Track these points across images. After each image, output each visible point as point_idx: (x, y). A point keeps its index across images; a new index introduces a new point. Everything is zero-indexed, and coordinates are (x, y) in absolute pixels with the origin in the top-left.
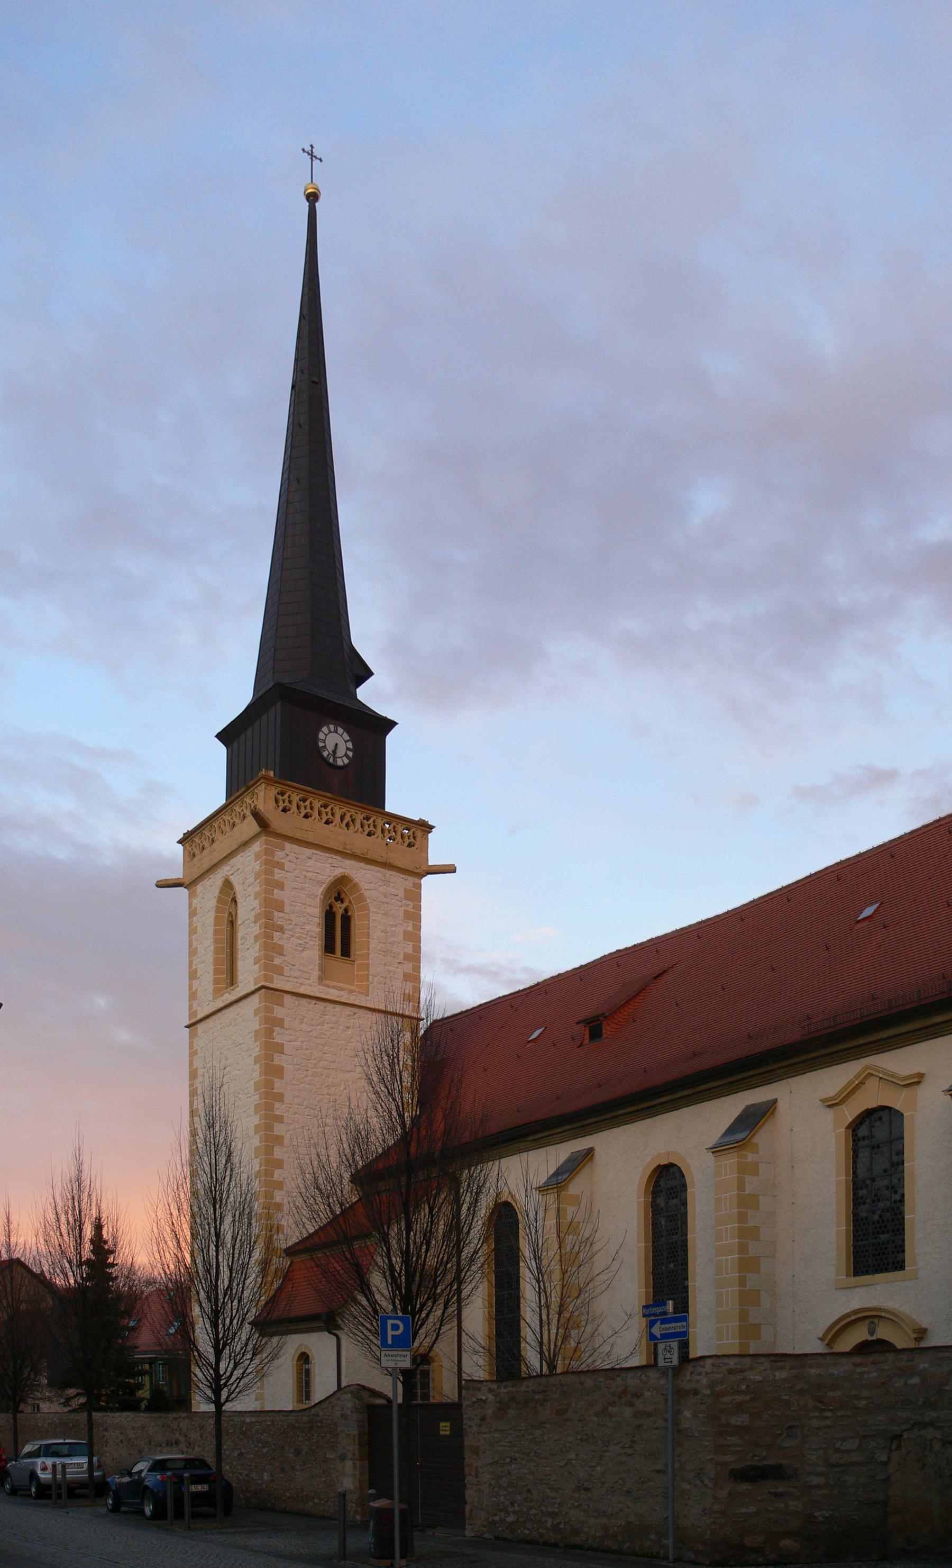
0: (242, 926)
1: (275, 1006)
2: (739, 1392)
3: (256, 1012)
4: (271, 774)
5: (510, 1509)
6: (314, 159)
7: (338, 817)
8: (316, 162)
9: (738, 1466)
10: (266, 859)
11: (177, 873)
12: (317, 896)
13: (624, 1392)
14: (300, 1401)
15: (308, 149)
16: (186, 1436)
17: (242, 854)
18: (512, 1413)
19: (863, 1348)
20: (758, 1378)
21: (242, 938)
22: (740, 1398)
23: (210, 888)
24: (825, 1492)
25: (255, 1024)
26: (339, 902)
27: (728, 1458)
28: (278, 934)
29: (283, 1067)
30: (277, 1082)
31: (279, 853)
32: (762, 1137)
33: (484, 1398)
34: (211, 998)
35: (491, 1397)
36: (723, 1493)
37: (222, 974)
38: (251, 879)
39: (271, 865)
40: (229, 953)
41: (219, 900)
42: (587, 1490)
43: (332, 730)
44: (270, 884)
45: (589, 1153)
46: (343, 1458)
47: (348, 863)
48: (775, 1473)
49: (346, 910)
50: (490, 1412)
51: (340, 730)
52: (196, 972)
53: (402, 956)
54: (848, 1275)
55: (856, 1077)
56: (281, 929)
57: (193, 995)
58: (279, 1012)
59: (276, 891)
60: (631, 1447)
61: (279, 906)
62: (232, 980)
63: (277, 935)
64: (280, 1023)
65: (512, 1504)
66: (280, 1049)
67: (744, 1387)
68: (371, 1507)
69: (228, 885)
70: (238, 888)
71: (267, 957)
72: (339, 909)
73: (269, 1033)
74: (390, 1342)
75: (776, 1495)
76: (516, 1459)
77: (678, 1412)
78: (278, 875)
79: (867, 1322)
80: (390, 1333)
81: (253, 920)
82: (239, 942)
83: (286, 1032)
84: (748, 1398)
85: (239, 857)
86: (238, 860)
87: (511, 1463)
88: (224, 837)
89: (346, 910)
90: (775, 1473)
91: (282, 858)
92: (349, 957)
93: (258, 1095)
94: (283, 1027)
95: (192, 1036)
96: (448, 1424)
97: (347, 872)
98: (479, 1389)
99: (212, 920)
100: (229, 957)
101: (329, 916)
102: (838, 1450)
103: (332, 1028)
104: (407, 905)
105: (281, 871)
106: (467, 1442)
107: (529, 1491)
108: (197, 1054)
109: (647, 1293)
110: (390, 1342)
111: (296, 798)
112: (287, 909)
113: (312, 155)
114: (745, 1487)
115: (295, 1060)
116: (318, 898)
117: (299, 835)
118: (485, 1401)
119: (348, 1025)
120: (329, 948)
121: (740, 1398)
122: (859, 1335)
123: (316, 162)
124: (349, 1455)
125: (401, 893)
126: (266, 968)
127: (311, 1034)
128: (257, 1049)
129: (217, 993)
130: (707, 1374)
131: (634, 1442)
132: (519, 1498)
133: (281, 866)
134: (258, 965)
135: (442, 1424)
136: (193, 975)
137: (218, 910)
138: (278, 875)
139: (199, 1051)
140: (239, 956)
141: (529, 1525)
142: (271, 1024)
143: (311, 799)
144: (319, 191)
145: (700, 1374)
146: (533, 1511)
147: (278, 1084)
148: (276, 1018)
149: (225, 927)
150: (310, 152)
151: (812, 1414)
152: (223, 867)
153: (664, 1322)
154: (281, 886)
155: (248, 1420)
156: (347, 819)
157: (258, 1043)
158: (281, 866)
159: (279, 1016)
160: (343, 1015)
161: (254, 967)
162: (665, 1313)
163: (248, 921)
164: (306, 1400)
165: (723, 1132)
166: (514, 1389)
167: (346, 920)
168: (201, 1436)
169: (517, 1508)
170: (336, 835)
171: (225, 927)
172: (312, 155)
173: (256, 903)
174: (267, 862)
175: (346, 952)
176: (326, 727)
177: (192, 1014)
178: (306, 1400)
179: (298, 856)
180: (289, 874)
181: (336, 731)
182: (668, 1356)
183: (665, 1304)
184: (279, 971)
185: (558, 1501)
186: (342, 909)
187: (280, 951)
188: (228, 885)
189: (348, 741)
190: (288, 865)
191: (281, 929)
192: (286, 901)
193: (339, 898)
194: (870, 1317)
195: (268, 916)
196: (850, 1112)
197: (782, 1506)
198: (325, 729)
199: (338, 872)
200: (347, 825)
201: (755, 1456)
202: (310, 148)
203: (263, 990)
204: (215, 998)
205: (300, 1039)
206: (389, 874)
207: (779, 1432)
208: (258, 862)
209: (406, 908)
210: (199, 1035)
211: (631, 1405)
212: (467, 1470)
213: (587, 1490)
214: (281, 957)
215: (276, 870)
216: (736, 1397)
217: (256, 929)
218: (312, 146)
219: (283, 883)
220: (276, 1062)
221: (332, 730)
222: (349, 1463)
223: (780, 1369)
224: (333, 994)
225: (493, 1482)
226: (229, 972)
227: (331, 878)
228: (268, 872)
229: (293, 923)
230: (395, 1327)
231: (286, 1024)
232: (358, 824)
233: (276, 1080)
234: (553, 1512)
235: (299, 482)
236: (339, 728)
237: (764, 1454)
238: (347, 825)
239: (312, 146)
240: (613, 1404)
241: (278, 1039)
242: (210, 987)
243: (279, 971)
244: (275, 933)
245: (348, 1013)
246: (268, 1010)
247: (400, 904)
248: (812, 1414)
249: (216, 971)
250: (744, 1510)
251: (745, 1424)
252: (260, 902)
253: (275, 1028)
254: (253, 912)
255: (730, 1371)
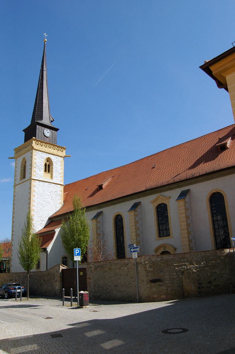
5: (98, 292)
9: (151, 279)
11: (13, 156)
14: (37, 269)
16: (15, 278)
18: (98, 269)
19: (163, 253)
20: (154, 260)
23: (20, 160)
24: (170, 285)
32: (138, 209)
33: (91, 266)
35: (93, 266)
36: (148, 286)
42: (117, 286)
45: (102, 212)
46: (56, 281)
48: (159, 280)
50: (93, 270)
54: (158, 237)
55: (157, 197)
57: (15, 180)
62: (24, 177)
65: (99, 291)
68: (87, 291)
74: (76, 255)
76: (99, 280)
79: (164, 247)
90: (159, 280)
95: (15, 188)
96: (82, 273)
97: (49, 157)
98: (90, 264)
102: (172, 275)
106: (87, 276)
109: (115, 242)
110: (76, 255)
118: (91, 267)
120: (45, 171)
122: (162, 250)
124: (58, 281)
129: (21, 180)
132: (100, 289)
135: (81, 273)
136: (15, 176)
141: (103, 295)
146: (104, 292)
151: (166, 268)
153: (133, 248)
155: (32, 274)
156: (50, 146)
165: (131, 207)
166: (98, 264)
168: (19, 278)
169: (100, 291)
170: (48, 150)
177: (15, 184)
185: (110, 289)
194: (164, 246)
196: (156, 204)
199: (47, 157)
211: (126, 266)
212: (87, 283)
213: (117, 286)
222: (58, 283)
225: (94, 286)
230: (77, 251)
234: (109, 292)
240: (122, 267)
248: (166, 268)
249: (21, 175)
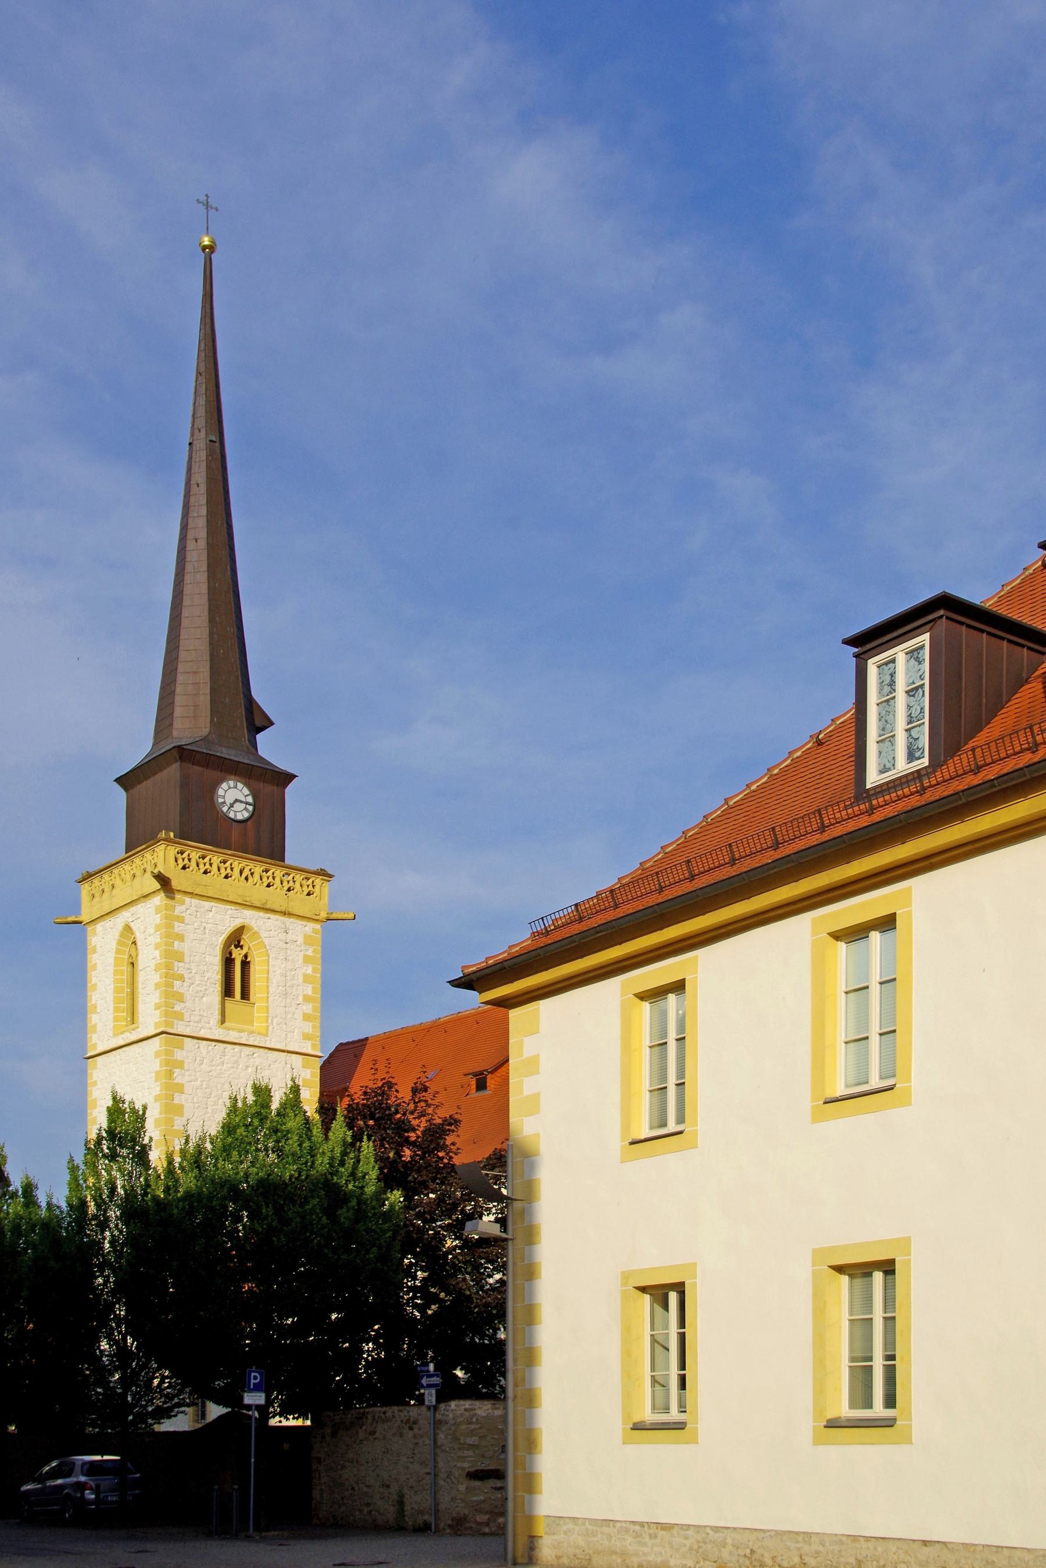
0: (143, 972)
1: (175, 1050)
2: (471, 1423)
3: (157, 1054)
4: (172, 834)
6: (209, 209)
7: (236, 872)
8: (212, 212)
10: (166, 914)
12: (216, 946)
13: (408, 1421)
15: (203, 199)
17: (143, 904)
20: (484, 1414)
21: (142, 984)
22: (473, 1427)
25: (156, 1065)
26: (239, 949)
27: (466, 1465)
28: (179, 982)
29: (183, 1105)
30: (178, 1119)
31: (179, 908)
34: (111, 1034)
37: (123, 1012)
38: (152, 931)
39: (171, 919)
40: (129, 993)
41: (120, 943)
43: (232, 786)
44: (171, 936)
47: (248, 913)
49: (246, 956)
51: (240, 785)
52: (96, 1007)
53: (301, 998)
56: (182, 978)
58: (179, 1055)
59: (176, 943)
60: (413, 1457)
61: (180, 957)
63: (177, 983)
64: (180, 1065)
66: (180, 1088)
67: (474, 1420)
69: (128, 928)
70: (139, 937)
71: (167, 1005)
72: (238, 955)
73: (170, 1074)
74: (252, 1387)
75: (496, 1489)
77: (435, 1435)
78: (178, 928)
80: (253, 1381)
81: (154, 968)
82: (140, 986)
83: (187, 1073)
84: (477, 1427)
85: (139, 906)
86: (140, 908)
87: (342, 1469)
88: (124, 886)
89: (246, 956)
91: (182, 912)
92: (249, 1000)
93: (158, 1132)
94: (182, 1068)
97: (247, 922)
99: (112, 961)
100: (129, 997)
101: (228, 962)
103: (232, 1068)
104: (307, 950)
105: (180, 924)
107: (353, 1488)
108: (96, 1085)
110: (252, 1387)
111: (195, 855)
112: (187, 960)
113: (207, 206)
114: (477, 1483)
115: (195, 1099)
116: (218, 948)
117: (197, 891)
119: (247, 1064)
120: (228, 991)
121: (473, 1427)
123: (212, 212)
125: (300, 940)
126: (166, 1014)
127: (211, 1074)
128: (158, 1089)
130: (452, 1411)
131: (414, 1454)
133: (181, 920)
134: (159, 1011)
137: (118, 951)
138: (178, 928)
139: (99, 1083)
140: (140, 1000)
142: (171, 1066)
143: (210, 856)
144: (215, 244)
145: (448, 1411)
147: (178, 1076)
148: (176, 1061)
149: (125, 968)
150: (205, 202)
152: (123, 913)
154: (181, 938)
156: (246, 872)
157: (158, 1083)
158: (181, 920)
159: (179, 1058)
160: (242, 1055)
161: (154, 1012)
162: (428, 1371)
163: (149, 968)
164: (202, 1419)
167: (245, 964)
170: (236, 887)
171: (125, 968)
172: (207, 206)
173: (157, 953)
174: (167, 917)
175: (245, 995)
176: (225, 783)
178: (202, 1419)
179: (198, 909)
180: (189, 927)
181: (236, 787)
182: (430, 1398)
183: (428, 1366)
184: (180, 1016)
186: (242, 956)
187: (181, 998)
188: (128, 928)
189: (247, 795)
190: (187, 919)
191: (182, 978)
192: (186, 952)
193: (238, 945)
195: (169, 967)
197: (500, 1496)
198: (224, 786)
199: (237, 923)
200: (247, 879)
201: (482, 1463)
202: (205, 198)
203: (164, 1035)
204: (115, 1035)
205: (199, 1080)
206: (289, 921)
207: (497, 1449)
208: (159, 915)
209: (305, 953)
210: (98, 1067)
213: (388, 1486)
214: (181, 1004)
215: (176, 924)
216: (470, 1426)
217: (156, 978)
218: (207, 196)
219: (183, 936)
220: (176, 1101)
221: (232, 786)
223: (498, 1409)
224: (232, 1036)
226: (129, 1011)
227: (231, 928)
228: (169, 926)
229: (193, 972)
230: (255, 1378)
231: (186, 1066)
232: (257, 877)
233: (176, 1118)
235: (196, 541)
236: (239, 784)
237: (488, 1463)
238: (247, 879)
239: (207, 196)
241: (178, 1080)
242: (111, 1024)
243: (180, 1016)
244: (175, 982)
245: (247, 1053)
246: (168, 1053)
247: (299, 949)
250: (475, 1499)
251: (476, 1443)
252: (160, 952)
253: (175, 1070)
254: (154, 961)
255: (466, 1410)
